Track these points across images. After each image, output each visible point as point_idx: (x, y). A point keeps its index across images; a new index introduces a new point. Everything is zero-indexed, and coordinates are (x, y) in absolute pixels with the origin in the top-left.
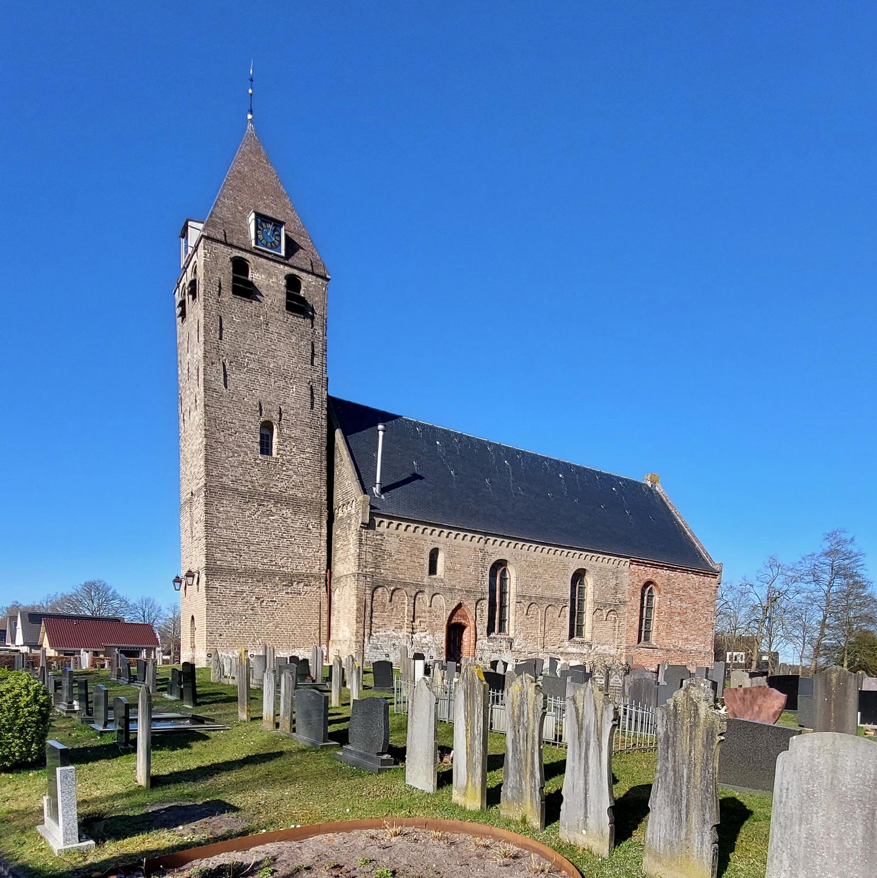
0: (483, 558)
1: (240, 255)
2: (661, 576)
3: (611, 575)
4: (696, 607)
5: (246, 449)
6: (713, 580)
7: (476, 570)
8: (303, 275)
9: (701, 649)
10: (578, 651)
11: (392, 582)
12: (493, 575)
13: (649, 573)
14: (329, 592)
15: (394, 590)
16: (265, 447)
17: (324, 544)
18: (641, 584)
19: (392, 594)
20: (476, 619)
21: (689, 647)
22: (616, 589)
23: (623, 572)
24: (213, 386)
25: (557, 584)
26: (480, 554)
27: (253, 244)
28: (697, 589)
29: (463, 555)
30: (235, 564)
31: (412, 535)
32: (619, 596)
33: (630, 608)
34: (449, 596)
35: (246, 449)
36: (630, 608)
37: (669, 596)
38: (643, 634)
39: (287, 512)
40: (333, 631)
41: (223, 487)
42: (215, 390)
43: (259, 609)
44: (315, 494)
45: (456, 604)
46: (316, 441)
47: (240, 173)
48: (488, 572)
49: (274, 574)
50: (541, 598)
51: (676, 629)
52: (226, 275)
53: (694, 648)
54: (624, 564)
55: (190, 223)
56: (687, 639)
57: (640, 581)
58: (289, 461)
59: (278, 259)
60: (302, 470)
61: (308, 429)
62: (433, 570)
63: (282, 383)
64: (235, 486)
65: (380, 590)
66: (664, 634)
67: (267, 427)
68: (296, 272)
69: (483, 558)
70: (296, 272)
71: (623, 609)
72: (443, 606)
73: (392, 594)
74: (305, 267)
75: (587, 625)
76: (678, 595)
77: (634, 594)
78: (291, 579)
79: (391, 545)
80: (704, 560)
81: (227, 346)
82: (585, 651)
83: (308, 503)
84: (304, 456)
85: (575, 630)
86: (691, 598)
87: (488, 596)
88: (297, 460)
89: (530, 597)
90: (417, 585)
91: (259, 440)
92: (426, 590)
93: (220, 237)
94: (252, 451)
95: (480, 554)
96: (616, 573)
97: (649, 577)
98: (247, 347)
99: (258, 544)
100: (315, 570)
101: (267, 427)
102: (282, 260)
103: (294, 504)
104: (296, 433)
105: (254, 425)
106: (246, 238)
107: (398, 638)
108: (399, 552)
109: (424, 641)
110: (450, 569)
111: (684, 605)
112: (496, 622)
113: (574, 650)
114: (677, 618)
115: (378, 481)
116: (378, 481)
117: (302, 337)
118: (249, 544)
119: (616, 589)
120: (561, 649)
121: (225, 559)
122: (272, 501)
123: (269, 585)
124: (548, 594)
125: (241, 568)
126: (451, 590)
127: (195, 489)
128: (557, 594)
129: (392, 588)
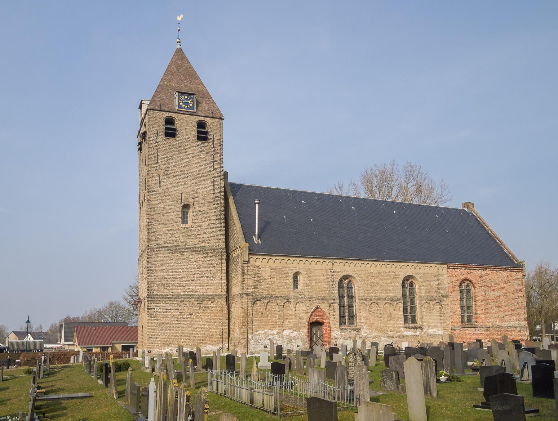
0: (332, 275)
1: (168, 115)
2: (474, 274)
3: (435, 277)
4: (508, 294)
5: (172, 222)
6: (518, 274)
7: (328, 284)
8: (207, 119)
9: (516, 325)
10: (413, 334)
11: (267, 297)
12: (340, 286)
13: (463, 273)
14: (228, 305)
15: (268, 302)
16: (185, 219)
17: (224, 275)
18: (459, 282)
19: (267, 305)
20: (332, 316)
21: (505, 324)
22: (439, 287)
23: (442, 275)
24: (153, 188)
25: (390, 288)
26: (330, 273)
27: (177, 108)
28: (506, 281)
29: (318, 274)
30: (166, 292)
31: (279, 265)
32: (442, 292)
33: (452, 299)
34: (308, 303)
35: (172, 222)
36: (452, 299)
37: (483, 288)
38: (467, 318)
39: (200, 256)
40: (231, 332)
41: (159, 246)
42: (154, 191)
43: (181, 320)
44: (217, 244)
45: (314, 308)
46: (217, 212)
47: (171, 72)
48: (337, 284)
49: (191, 296)
50: (379, 299)
51: (492, 312)
52: (161, 127)
53: (510, 325)
54: (443, 269)
55: (143, 102)
56: (503, 318)
57: (458, 280)
58: (200, 226)
59: (192, 113)
60: (208, 230)
61: (212, 206)
62: (296, 286)
63: (194, 181)
64: (167, 244)
65: (259, 303)
66: (483, 316)
67: (186, 207)
68: (202, 118)
69: (332, 275)
70: (202, 118)
71: (445, 301)
72: (303, 312)
73: (267, 305)
74: (208, 115)
75: (418, 314)
76: (491, 287)
77: (453, 289)
78: (202, 299)
79: (265, 273)
80: (510, 260)
81: (161, 166)
82: (418, 333)
83: (212, 250)
84: (210, 222)
85: (410, 317)
86: (502, 288)
87: (338, 301)
88: (206, 224)
89: (371, 299)
90: (284, 298)
91: (181, 216)
92: (292, 301)
93: (156, 108)
94: (177, 223)
95: (330, 273)
96: (437, 276)
97: (465, 276)
98: (174, 164)
99: (181, 278)
100: (219, 292)
101: (186, 207)
102: (194, 114)
103: (204, 251)
104: (204, 208)
105: (179, 208)
106: (173, 106)
107: (273, 334)
108: (270, 277)
109: (292, 335)
110: (308, 285)
111: (497, 294)
112: (347, 318)
113: (410, 333)
114: (493, 304)
115: (257, 232)
116: (257, 232)
117: (207, 154)
118: (175, 279)
119: (439, 287)
120: (399, 334)
121: (160, 290)
122: (190, 251)
123: (188, 304)
124: (384, 295)
125: (170, 295)
126: (310, 299)
127: (144, 248)
128: (392, 295)
129: (267, 301)
